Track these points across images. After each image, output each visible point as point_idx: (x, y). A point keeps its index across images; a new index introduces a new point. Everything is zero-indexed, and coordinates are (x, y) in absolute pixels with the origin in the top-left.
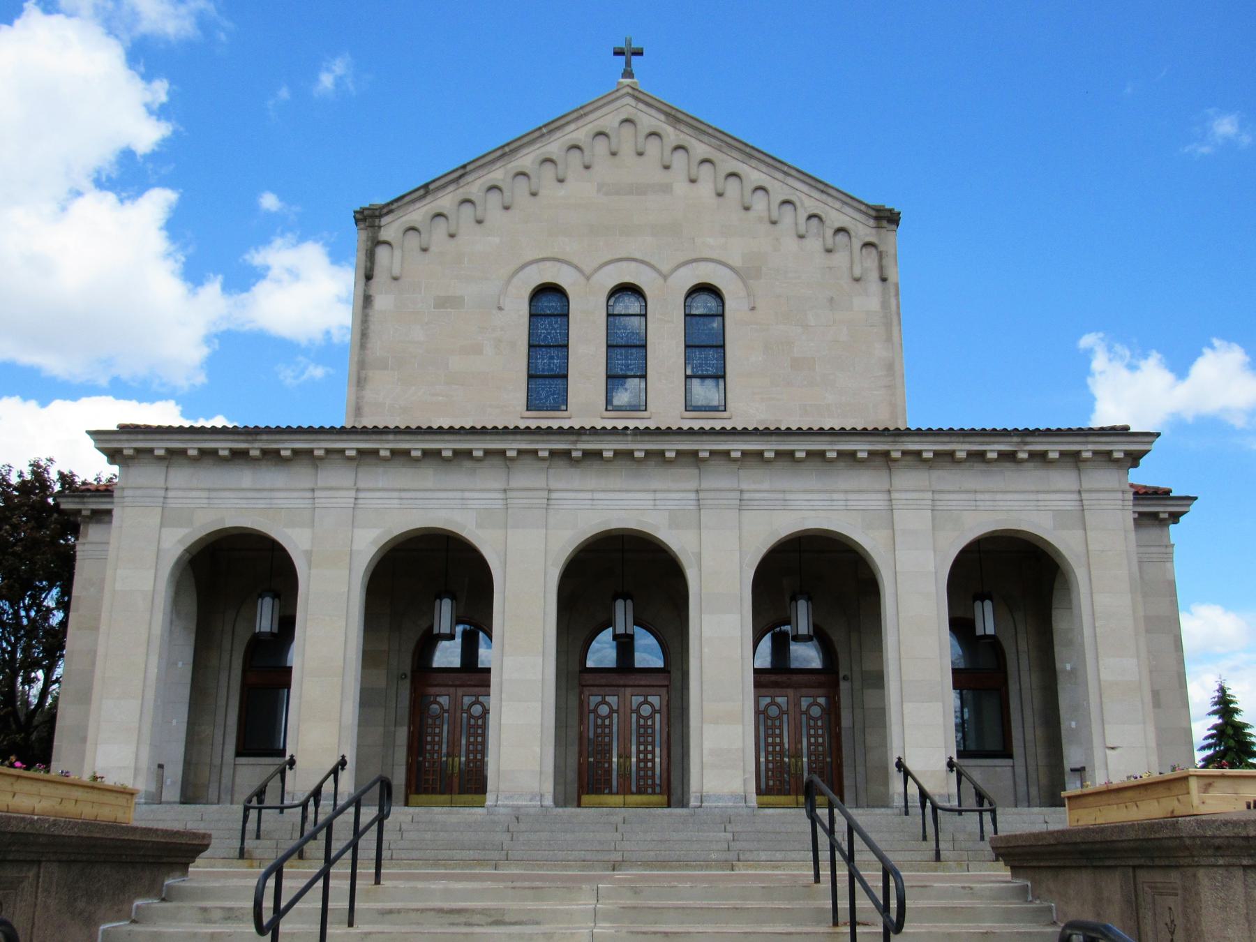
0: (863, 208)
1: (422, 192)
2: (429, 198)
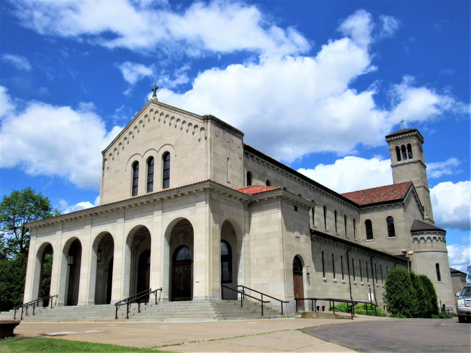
0: (200, 117)
1: (112, 144)
2: (114, 145)
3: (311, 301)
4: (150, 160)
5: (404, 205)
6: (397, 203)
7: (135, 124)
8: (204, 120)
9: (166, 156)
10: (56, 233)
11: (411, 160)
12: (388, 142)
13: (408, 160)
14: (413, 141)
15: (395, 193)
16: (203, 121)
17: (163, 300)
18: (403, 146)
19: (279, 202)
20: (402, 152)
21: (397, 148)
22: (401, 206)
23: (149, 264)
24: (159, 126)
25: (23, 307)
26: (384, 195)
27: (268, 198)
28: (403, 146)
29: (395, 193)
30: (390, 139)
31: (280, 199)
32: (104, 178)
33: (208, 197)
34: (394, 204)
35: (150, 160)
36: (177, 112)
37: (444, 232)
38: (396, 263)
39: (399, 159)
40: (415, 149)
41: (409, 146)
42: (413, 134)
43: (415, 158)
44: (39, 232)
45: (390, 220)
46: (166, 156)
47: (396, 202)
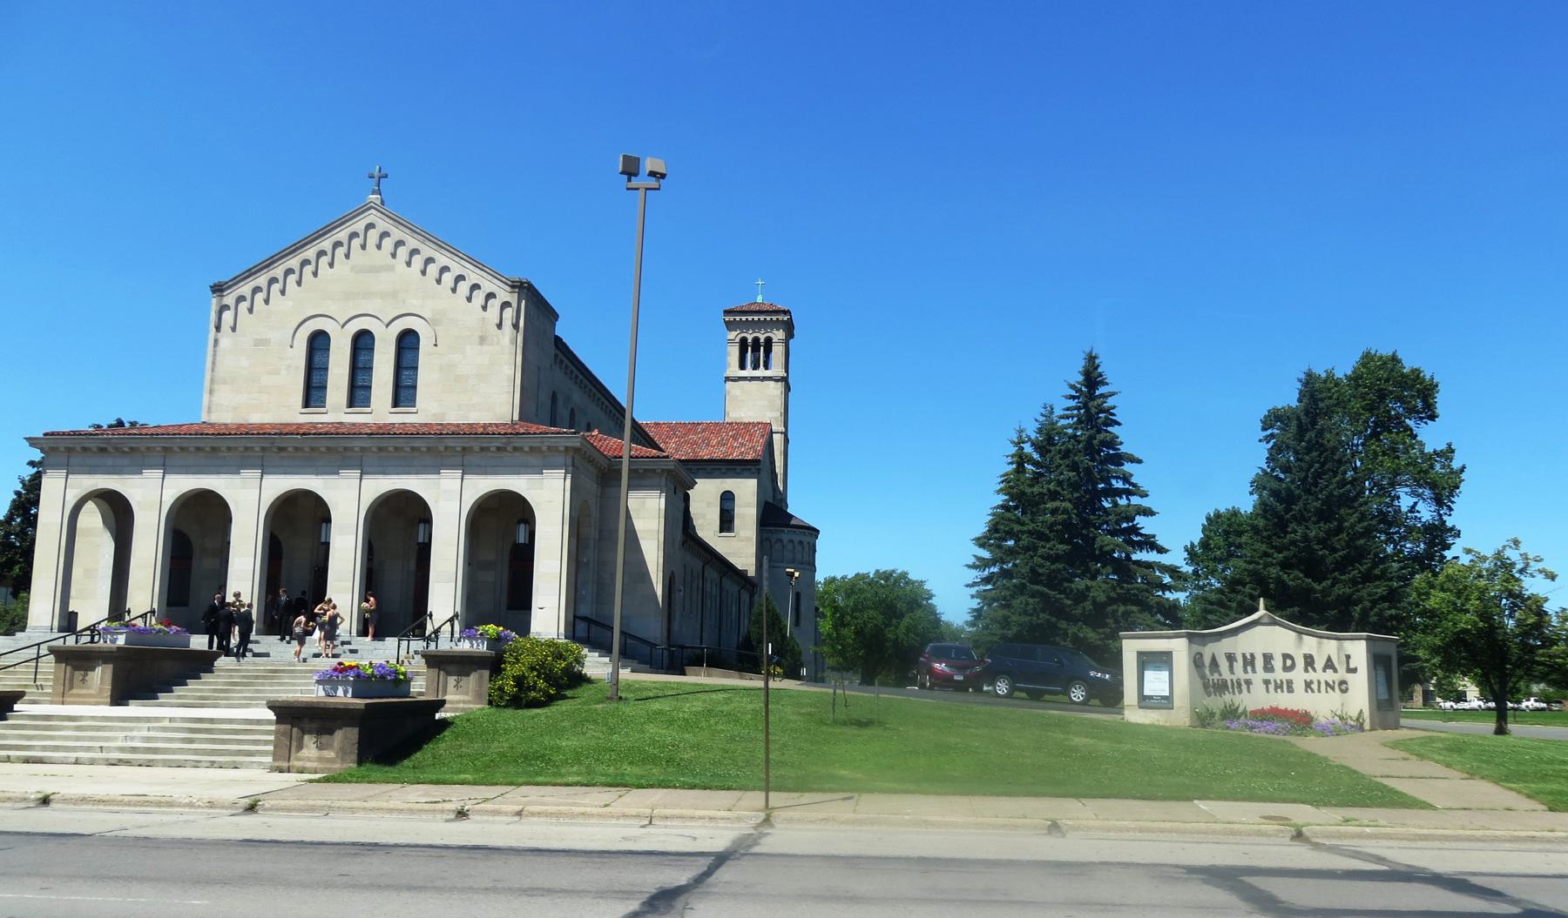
3: (680, 650)
4: (363, 343)
5: (759, 473)
6: (748, 467)
7: (320, 245)
8: (513, 287)
9: (407, 342)
10: (141, 473)
11: (768, 373)
12: (728, 324)
13: (761, 372)
14: (777, 335)
15: (742, 444)
16: (508, 289)
17: (367, 636)
18: (756, 340)
19: (664, 480)
20: (752, 351)
21: (743, 342)
22: (753, 473)
23: (229, 543)
24: (391, 268)
25: (409, 641)
26: (718, 443)
27: (645, 470)
28: (756, 340)
29: (742, 444)
30: (732, 319)
31: (665, 475)
32: (218, 349)
33: (569, 461)
34: (728, 467)
35: (363, 343)
36: (443, 251)
37: (813, 533)
38: (742, 588)
39: (742, 366)
40: (778, 351)
41: (769, 341)
42: (780, 318)
43: (777, 370)
44: (73, 461)
45: (727, 498)
46: (407, 342)
47: (745, 465)
